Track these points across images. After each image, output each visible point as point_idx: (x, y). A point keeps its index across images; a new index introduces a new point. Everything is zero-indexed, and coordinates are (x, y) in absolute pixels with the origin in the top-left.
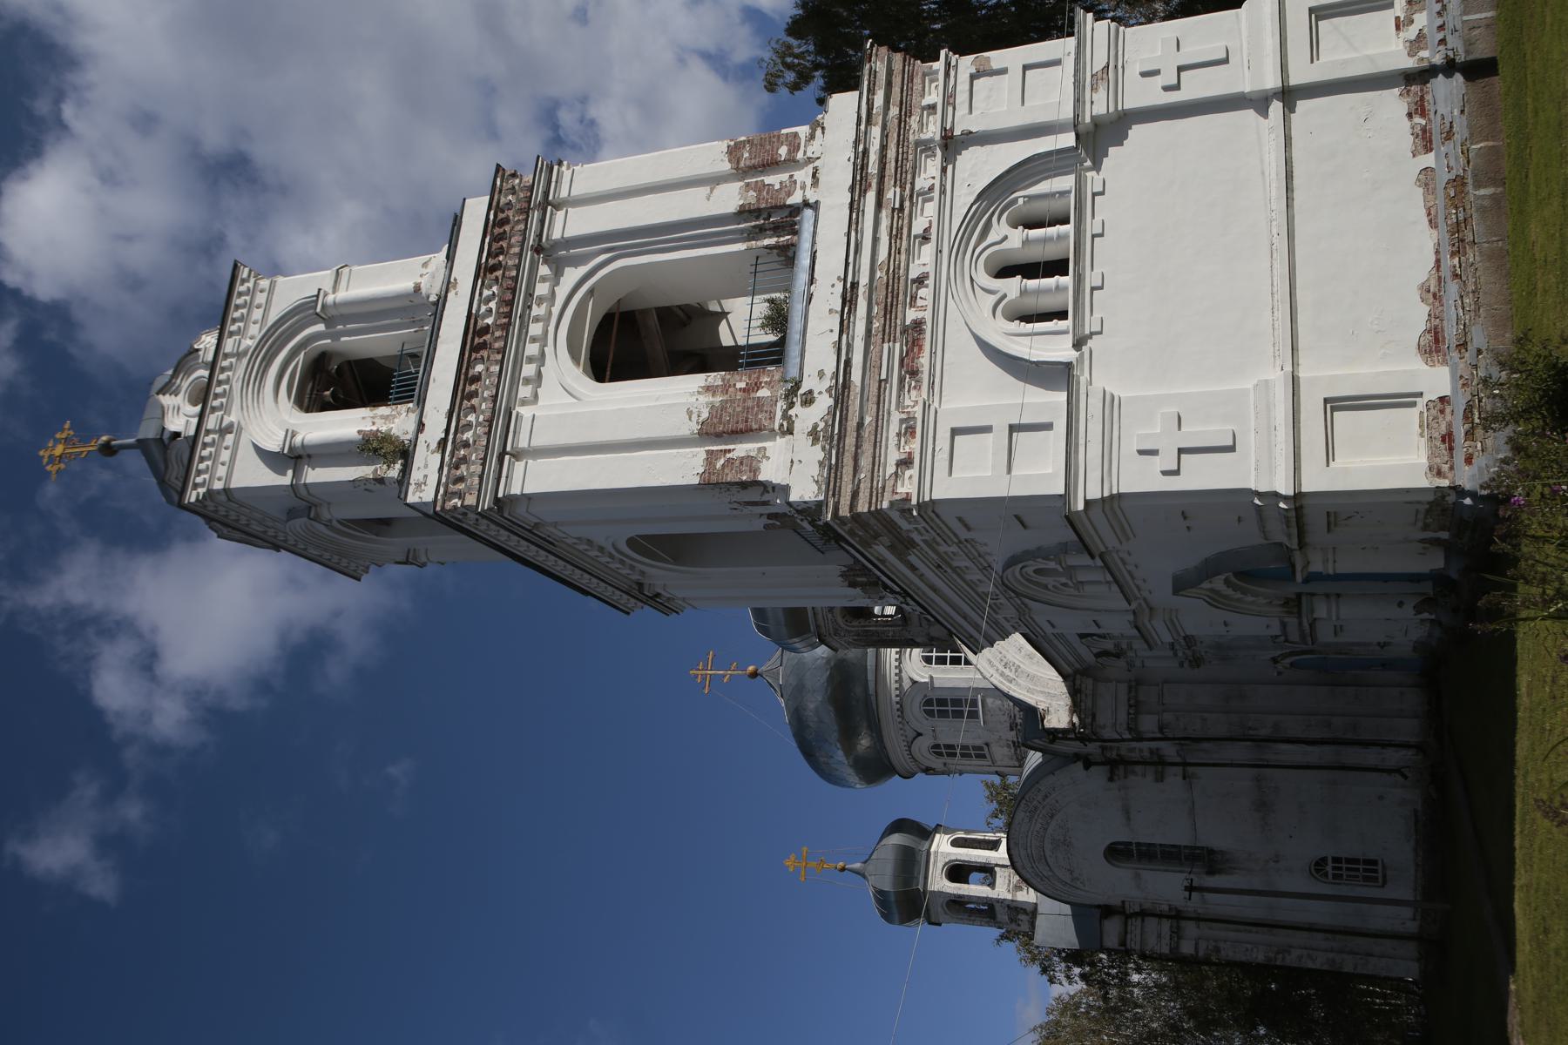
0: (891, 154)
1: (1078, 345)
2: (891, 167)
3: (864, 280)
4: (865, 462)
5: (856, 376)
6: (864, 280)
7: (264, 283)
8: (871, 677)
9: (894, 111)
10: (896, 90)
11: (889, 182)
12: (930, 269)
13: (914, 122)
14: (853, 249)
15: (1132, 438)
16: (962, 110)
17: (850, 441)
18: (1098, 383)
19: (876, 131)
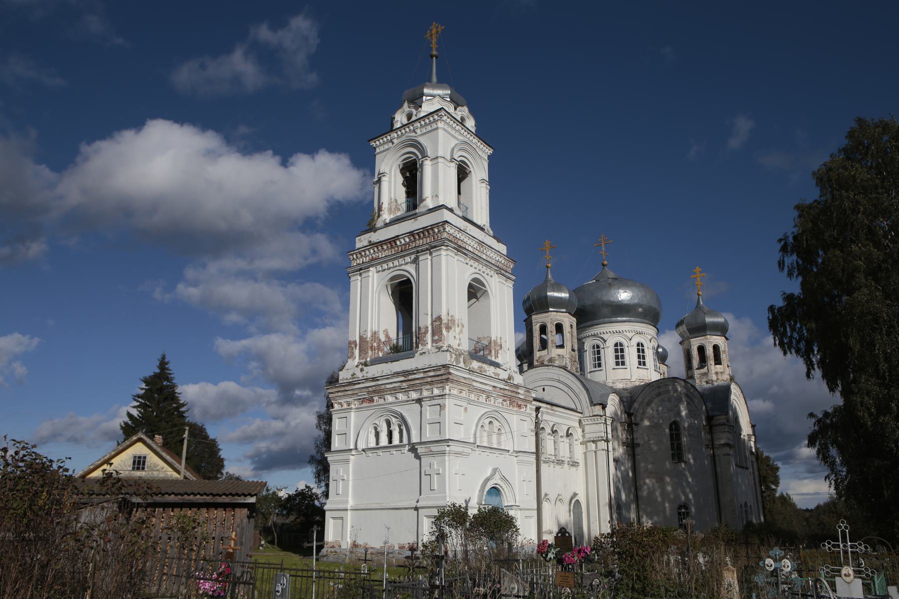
0: (417, 382)
1: (363, 450)
2: (413, 383)
3: (380, 383)
4: (340, 394)
5: (357, 386)
6: (380, 383)
7: (9, 469)
8: (614, 319)
9: (429, 379)
10: (437, 378)
11: (408, 383)
12: (387, 401)
13: (428, 387)
14: (387, 377)
15: (435, 461)
16: (429, 403)
17: (343, 389)
18: (352, 457)
19: (422, 375)
